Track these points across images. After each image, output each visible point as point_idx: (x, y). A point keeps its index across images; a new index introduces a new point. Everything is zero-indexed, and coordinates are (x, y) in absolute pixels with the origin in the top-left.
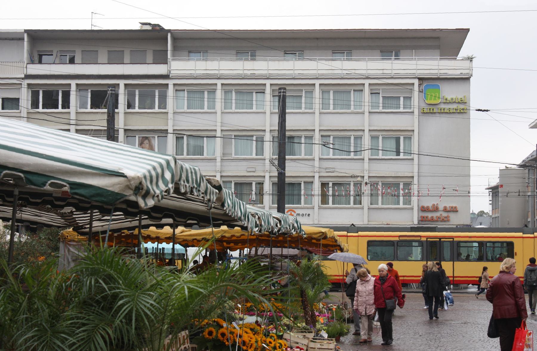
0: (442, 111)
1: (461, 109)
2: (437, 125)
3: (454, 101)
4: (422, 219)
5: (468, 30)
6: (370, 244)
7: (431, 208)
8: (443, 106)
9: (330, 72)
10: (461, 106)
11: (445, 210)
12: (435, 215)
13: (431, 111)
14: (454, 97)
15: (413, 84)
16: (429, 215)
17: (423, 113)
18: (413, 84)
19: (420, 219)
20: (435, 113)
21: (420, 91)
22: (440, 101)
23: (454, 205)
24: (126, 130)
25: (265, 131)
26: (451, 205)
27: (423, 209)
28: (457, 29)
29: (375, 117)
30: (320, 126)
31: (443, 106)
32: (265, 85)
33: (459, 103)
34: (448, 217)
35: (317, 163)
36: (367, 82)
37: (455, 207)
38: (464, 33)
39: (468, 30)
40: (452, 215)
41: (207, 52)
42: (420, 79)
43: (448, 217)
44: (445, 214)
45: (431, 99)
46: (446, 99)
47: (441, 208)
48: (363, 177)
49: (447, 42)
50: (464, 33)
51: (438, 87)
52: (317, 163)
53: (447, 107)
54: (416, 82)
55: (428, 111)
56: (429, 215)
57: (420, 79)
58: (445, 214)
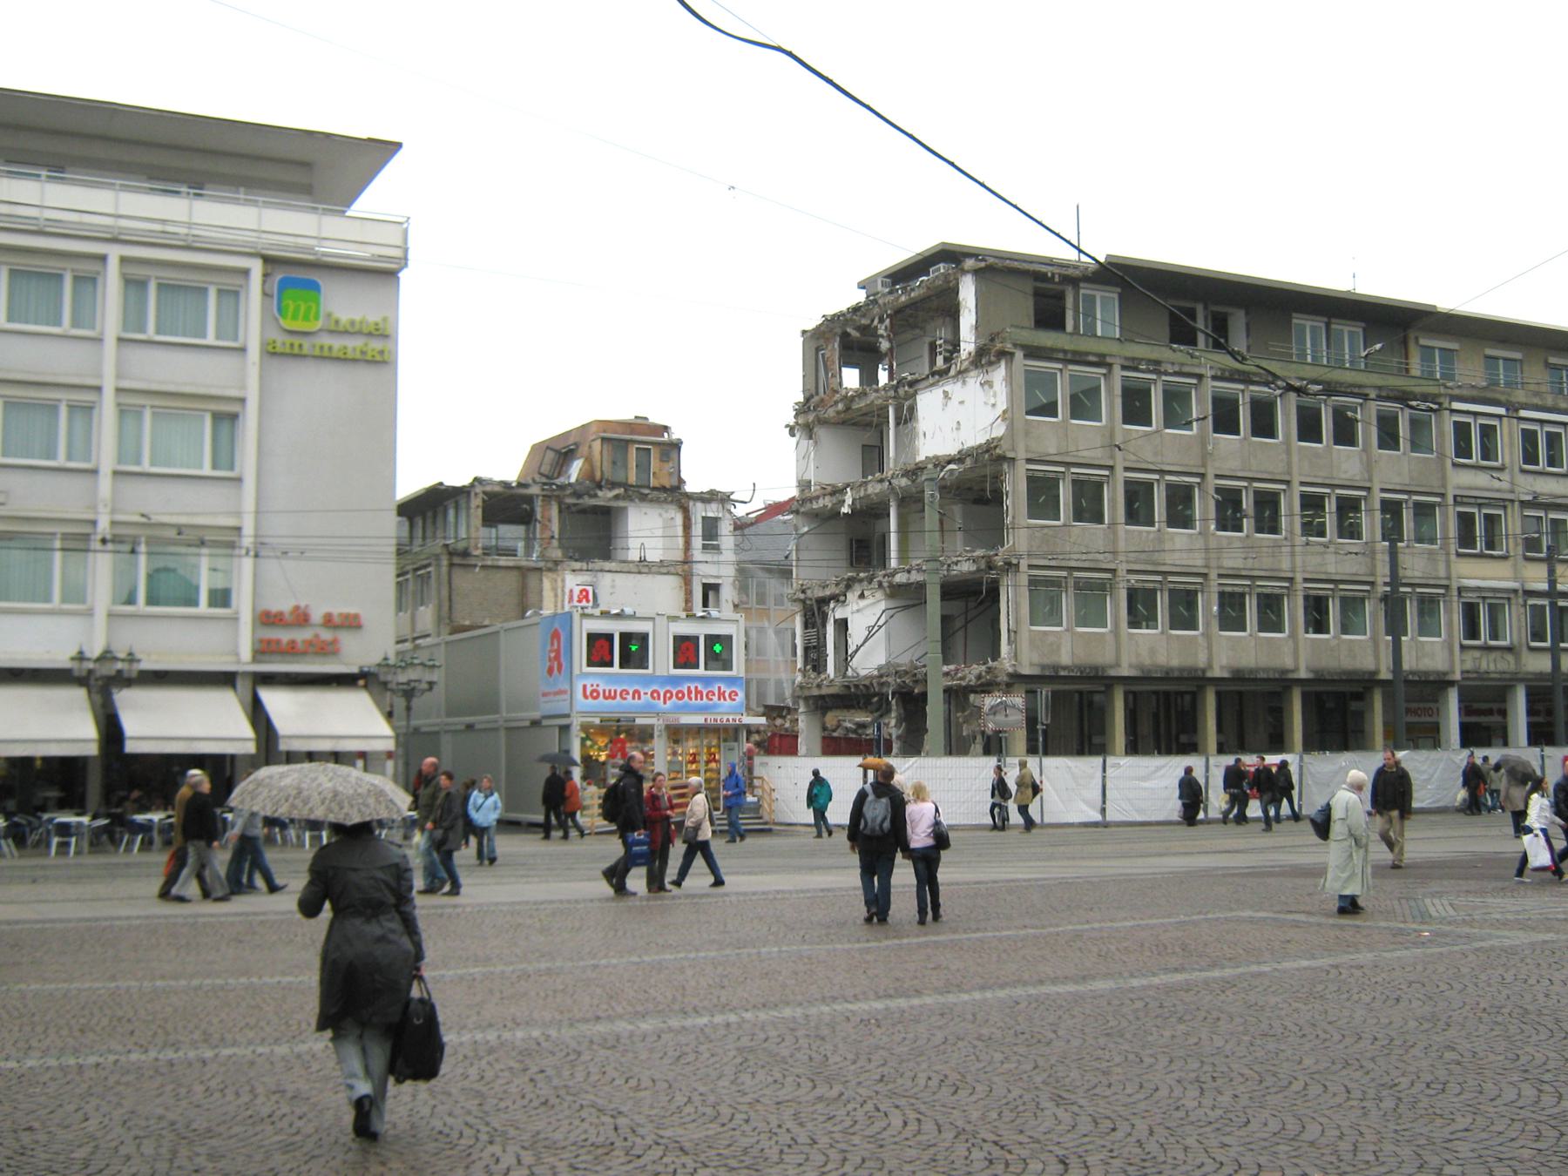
0: (326, 353)
1: (373, 352)
2: (315, 391)
3: (357, 328)
4: (263, 650)
5: (396, 147)
6: (1134, 624)
7: (288, 617)
8: (327, 341)
9: (74, 217)
10: (375, 345)
11: (328, 621)
12: (301, 635)
13: (296, 351)
14: (358, 318)
15: (246, 273)
16: (284, 636)
17: (271, 353)
18: (246, 273)
19: (258, 646)
20: (305, 356)
21: (265, 294)
22: (319, 325)
23: (352, 610)
24: (119, 391)
25: (98, 389)
26: (346, 610)
27: (267, 619)
28: (370, 140)
29: (137, 355)
30: (119, 376)
31: (327, 341)
32: (103, 259)
33: (370, 334)
34: (335, 641)
35: (105, 484)
36: (114, 253)
37: (356, 616)
38: (377, 153)
39: (396, 147)
40: (348, 641)
41: (61, 169)
42: (268, 260)
43: (335, 641)
44: (326, 635)
45: (295, 317)
46: (337, 322)
47: (317, 616)
48: (94, 523)
49: (318, 166)
50: (377, 153)
51: (314, 287)
52: (105, 484)
53: (337, 343)
54: (256, 267)
55: (288, 350)
56: (284, 636)
57: (268, 260)
58: (326, 635)
